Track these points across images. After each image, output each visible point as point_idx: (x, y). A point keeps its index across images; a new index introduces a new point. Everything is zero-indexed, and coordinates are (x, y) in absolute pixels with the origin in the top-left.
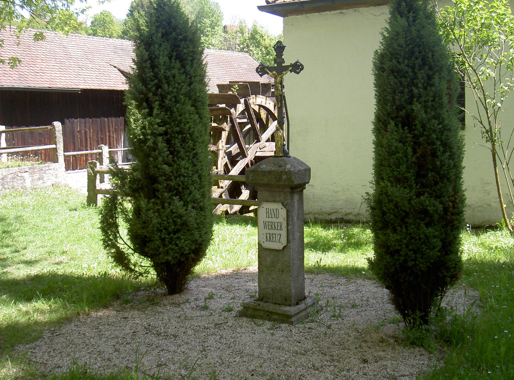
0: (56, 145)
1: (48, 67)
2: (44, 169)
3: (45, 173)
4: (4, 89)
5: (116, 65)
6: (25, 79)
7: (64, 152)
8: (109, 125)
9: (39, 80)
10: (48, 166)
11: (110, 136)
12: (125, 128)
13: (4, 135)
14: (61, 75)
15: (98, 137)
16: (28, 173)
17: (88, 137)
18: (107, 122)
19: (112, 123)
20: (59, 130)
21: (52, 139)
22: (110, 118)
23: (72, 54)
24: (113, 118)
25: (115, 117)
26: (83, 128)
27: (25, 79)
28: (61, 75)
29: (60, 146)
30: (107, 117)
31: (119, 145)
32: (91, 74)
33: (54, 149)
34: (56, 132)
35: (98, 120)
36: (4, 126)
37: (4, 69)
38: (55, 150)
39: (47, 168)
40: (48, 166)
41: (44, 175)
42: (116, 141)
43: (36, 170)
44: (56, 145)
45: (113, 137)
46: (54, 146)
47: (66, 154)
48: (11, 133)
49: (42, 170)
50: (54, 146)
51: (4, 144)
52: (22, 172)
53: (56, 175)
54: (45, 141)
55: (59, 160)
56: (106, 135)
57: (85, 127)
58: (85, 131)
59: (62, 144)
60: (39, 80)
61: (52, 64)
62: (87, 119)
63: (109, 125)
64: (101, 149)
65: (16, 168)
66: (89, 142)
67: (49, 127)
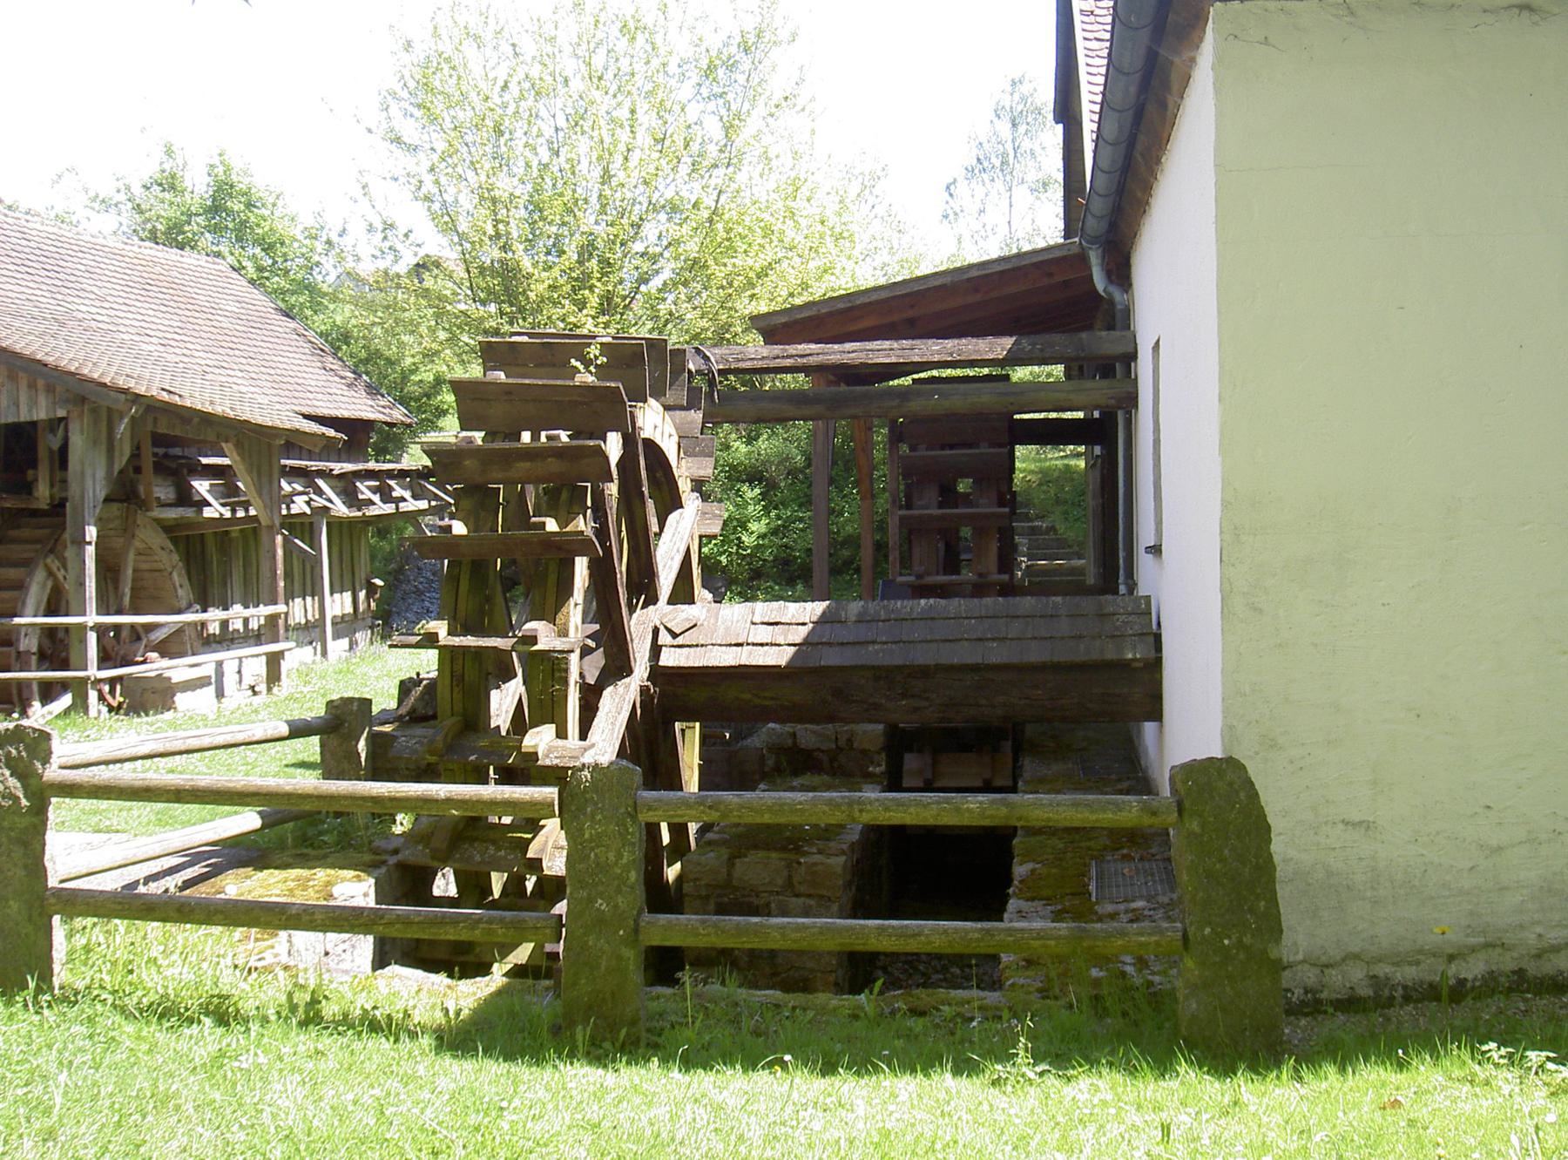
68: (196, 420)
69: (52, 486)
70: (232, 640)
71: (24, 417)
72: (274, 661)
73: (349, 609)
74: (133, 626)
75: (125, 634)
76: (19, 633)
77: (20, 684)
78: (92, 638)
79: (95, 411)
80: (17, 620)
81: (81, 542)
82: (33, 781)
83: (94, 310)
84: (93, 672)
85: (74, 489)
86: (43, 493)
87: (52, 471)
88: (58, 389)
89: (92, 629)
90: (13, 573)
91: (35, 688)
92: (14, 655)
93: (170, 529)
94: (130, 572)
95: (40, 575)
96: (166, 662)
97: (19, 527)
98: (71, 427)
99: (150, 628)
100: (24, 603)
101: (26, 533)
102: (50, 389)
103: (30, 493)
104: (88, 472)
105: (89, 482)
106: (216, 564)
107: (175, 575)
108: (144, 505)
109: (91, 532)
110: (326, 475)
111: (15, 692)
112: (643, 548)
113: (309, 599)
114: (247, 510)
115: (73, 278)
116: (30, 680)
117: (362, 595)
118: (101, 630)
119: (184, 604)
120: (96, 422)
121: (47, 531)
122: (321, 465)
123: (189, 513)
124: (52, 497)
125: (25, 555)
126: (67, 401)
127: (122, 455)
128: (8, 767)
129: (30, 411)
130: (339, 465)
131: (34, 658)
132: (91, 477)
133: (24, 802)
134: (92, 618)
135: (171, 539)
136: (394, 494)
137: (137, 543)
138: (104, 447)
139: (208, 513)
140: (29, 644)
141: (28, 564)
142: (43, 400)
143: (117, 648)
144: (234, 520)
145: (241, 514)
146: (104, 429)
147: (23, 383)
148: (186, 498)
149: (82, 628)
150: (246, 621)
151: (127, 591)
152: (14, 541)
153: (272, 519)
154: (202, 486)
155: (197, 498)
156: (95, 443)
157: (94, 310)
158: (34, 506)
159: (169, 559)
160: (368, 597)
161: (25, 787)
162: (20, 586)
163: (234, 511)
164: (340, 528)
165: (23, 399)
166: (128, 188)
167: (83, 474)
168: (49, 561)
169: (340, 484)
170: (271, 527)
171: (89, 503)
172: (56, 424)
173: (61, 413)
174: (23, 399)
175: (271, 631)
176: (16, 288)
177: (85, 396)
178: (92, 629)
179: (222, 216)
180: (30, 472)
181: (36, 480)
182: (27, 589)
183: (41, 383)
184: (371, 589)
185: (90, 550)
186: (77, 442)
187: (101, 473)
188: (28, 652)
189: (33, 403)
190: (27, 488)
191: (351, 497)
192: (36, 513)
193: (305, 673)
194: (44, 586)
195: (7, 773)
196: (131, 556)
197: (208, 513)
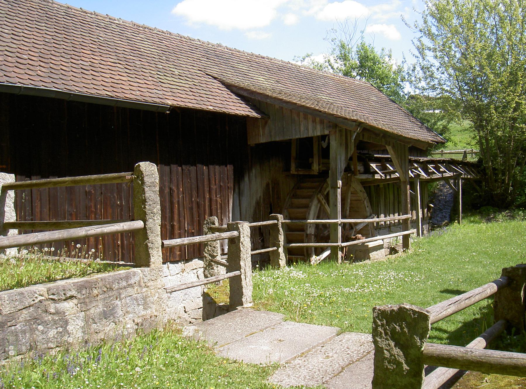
0: (145, 222)
1: (103, 62)
2: (115, 286)
3: (118, 297)
4: (16, 92)
5: (216, 76)
6: (61, 76)
7: (163, 237)
8: (209, 180)
9: (89, 82)
10: (127, 278)
11: (210, 200)
12: (234, 186)
13: (11, 193)
14: (129, 79)
15: (192, 202)
16: (75, 301)
17: (175, 200)
18: (193, 175)
19: (215, 175)
20: (153, 184)
21: (135, 209)
22: (211, 167)
23: (143, 50)
24: (217, 167)
25: (220, 164)
26: (167, 184)
27: (61, 76)
28: (129, 79)
29: (155, 223)
30: (207, 165)
31: (225, 216)
32: (181, 84)
33: (133, 233)
34: (146, 189)
35: (193, 168)
36: (13, 176)
37: (19, 55)
38: (143, 232)
39: (124, 284)
40: (127, 278)
41: (118, 302)
42: (221, 208)
43: (95, 292)
44: (145, 222)
45: (217, 201)
46: (139, 224)
47: (167, 242)
48: (28, 189)
49: (111, 289)
50: (139, 224)
51: (10, 215)
52: (60, 300)
53: (145, 298)
54: (96, 208)
55: (152, 260)
56: (204, 198)
57: (171, 181)
58: (171, 189)
59: (158, 219)
60: (89, 82)
61: (112, 60)
62: (174, 167)
63: (209, 180)
64: (237, 229)
65: (41, 288)
66: (176, 211)
67: (128, 175)
68: (382, 135)
69: (319, 165)
70: (380, 229)
71: (310, 134)
72: (406, 238)
74: (350, 224)
75: (347, 227)
76: (307, 226)
77: (308, 248)
78: (340, 229)
79: (340, 131)
80: (309, 221)
81: (335, 187)
82: (412, 351)
83: (327, 98)
84: (340, 243)
85: (332, 165)
86: (316, 168)
87: (319, 159)
88: (325, 121)
89: (340, 225)
90: (304, 201)
91: (313, 249)
92: (305, 235)
93: (363, 183)
94: (349, 201)
95: (315, 202)
96: (364, 240)
98: (331, 138)
99: (356, 224)
100: (309, 213)
102: (322, 122)
103: (311, 168)
104: (338, 157)
105: (339, 161)
106: (383, 197)
107: (365, 202)
108: (354, 173)
109: (340, 183)
110: (417, 162)
111: (305, 251)
112: (18, 212)
114: (390, 176)
115: (318, 87)
116: (312, 247)
117: (426, 210)
118: (344, 225)
119: (368, 214)
120: (341, 136)
121: (317, 184)
122: (416, 158)
123: (369, 176)
124: (319, 169)
125: (308, 194)
126: (330, 126)
127: (351, 150)
128: (393, 339)
129: (313, 132)
130: (422, 158)
131: (313, 236)
132: (339, 158)
133: (405, 367)
134: (340, 220)
135: (364, 187)
136: (441, 170)
137: (352, 189)
138: (344, 148)
139: (377, 177)
140: (311, 231)
141: (310, 197)
142: (318, 127)
143: (349, 232)
144: (386, 180)
145: (388, 177)
146: (344, 138)
147: (310, 121)
148: (368, 170)
149: (336, 224)
150: (385, 222)
151: (348, 209)
153: (406, 178)
154: (373, 166)
155: (372, 171)
156: (341, 144)
157: (327, 98)
158: (312, 173)
159: (363, 195)
160: (428, 211)
161: (406, 355)
162: (307, 207)
163: (386, 176)
164: (425, 183)
165: (310, 127)
166: (329, 61)
167: (336, 158)
168: (319, 196)
169: (422, 166)
170: (405, 182)
171: (339, 170)
172: (323, 137)
173: (326, 132)
174: (310, 127)
175: (404, 225)
176: (299, 89)
177: (336, 123)
178: (340, 225)
179: (367, 65)
180: (310, 159)
181: (313, 162)
182: (310, 207)
183: (318, 119)
184: (429, 208)
185: (339, 191)
186: (334, 144)
187: (343, 158)
188: (311, 234)
189: (315, 128)
190: (309, 166)
191: (426, 170)
192: (314, 176)
193: (418, 245)
194: (317, 207)
195: (392, 344)
196: (350, 194)
197: (377, 177)
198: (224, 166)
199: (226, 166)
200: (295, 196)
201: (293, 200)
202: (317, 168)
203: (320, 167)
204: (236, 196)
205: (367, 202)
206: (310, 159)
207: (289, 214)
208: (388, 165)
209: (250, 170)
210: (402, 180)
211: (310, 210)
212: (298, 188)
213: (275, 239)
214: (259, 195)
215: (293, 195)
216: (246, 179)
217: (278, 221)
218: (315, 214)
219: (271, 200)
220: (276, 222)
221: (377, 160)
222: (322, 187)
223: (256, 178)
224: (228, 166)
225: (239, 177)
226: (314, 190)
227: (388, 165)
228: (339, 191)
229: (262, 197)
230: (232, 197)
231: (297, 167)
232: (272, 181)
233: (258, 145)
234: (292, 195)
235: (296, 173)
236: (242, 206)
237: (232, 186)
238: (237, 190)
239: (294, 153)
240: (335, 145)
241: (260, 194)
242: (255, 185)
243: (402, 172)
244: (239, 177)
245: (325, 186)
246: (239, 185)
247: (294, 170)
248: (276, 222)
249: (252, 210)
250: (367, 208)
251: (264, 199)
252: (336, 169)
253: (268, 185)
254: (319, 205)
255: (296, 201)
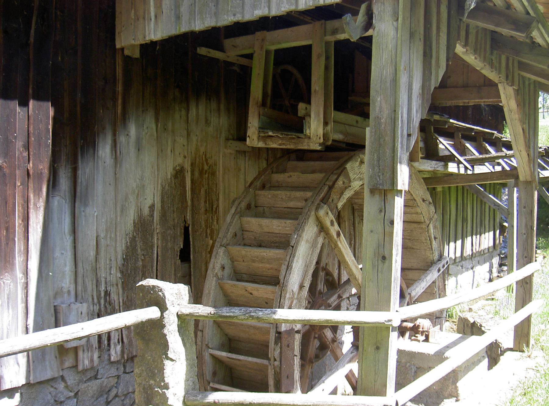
69: (326, 124)
73: (491, 244)
80: (282, 314)
81: (385, 190)
86: (316, 130)
90: (276, 226)
95: (310, 230)
97: (284, 171)
100: (289, 267)
101: (294, 177)
103: (302, 132)
104: (403, 80)
107: (431, 226)
113: (474, 237)
121: (319, 176)
125: (291, 204)
127: (438, 66)
138: (420, 46)
141: (296, 215)
152: (278, 187)
156: (412, 35)
160: (500, 235)
167: (395, 81)
168: (321, 213)
171: (402, 130)
180: (301, 106)
182: (294, 248)
185: (399, 202)
190: (297, 126)
192: (302, 155)
194: (313, 245)
198: (14, 104)
199: (24, 103)
200: (253, 209)
201: (245, 219)
202: (321, 132)
203: (329, 128)
204: (61, 203)
205: (435, 227)
206: (301, 106)
207: (232, 260)
208: (468, 145)
209: (119, 123)
210: (521, 178)
211: (293, 255)
212: (263, 187)
213: (153, 376)
214: (149, 202)
215: (249, 207)
216: (104, 150)
217: (163, 308)
218: (307, 266)
219: (189, 217)
220: (153, 313)
221: (449, 134)
222: (331, 188)
223: (139, 148)
224: (31, 103)
225: (73, 141)
226: (309, 194)
227: (468, 145)
228: (399, 202)
229: (158, 205)
230: (41, 204)
231: (262, 128)
232: (192, 165)
233: (148, 48)
234: (243, 205)
235: (261, 145)
236: (80, 235)
237: (44, 167)
238: (64, 183)
239: (256, 90)
240: (392, 33)
241: (152, 196)
242: (134, 169)
243: (526, 158)
244: (73, 141)
245: (340, 183)
246: (75, 171)
247: (255, 137)
248: (153, 313)
249: (121, 247)
250: (434, 242)
251: (164, 215)
252: (394, 121)
253: (179, 173)
254: (320, 240)
255: (256, 225)
